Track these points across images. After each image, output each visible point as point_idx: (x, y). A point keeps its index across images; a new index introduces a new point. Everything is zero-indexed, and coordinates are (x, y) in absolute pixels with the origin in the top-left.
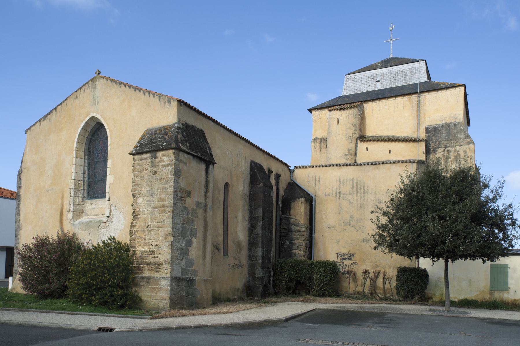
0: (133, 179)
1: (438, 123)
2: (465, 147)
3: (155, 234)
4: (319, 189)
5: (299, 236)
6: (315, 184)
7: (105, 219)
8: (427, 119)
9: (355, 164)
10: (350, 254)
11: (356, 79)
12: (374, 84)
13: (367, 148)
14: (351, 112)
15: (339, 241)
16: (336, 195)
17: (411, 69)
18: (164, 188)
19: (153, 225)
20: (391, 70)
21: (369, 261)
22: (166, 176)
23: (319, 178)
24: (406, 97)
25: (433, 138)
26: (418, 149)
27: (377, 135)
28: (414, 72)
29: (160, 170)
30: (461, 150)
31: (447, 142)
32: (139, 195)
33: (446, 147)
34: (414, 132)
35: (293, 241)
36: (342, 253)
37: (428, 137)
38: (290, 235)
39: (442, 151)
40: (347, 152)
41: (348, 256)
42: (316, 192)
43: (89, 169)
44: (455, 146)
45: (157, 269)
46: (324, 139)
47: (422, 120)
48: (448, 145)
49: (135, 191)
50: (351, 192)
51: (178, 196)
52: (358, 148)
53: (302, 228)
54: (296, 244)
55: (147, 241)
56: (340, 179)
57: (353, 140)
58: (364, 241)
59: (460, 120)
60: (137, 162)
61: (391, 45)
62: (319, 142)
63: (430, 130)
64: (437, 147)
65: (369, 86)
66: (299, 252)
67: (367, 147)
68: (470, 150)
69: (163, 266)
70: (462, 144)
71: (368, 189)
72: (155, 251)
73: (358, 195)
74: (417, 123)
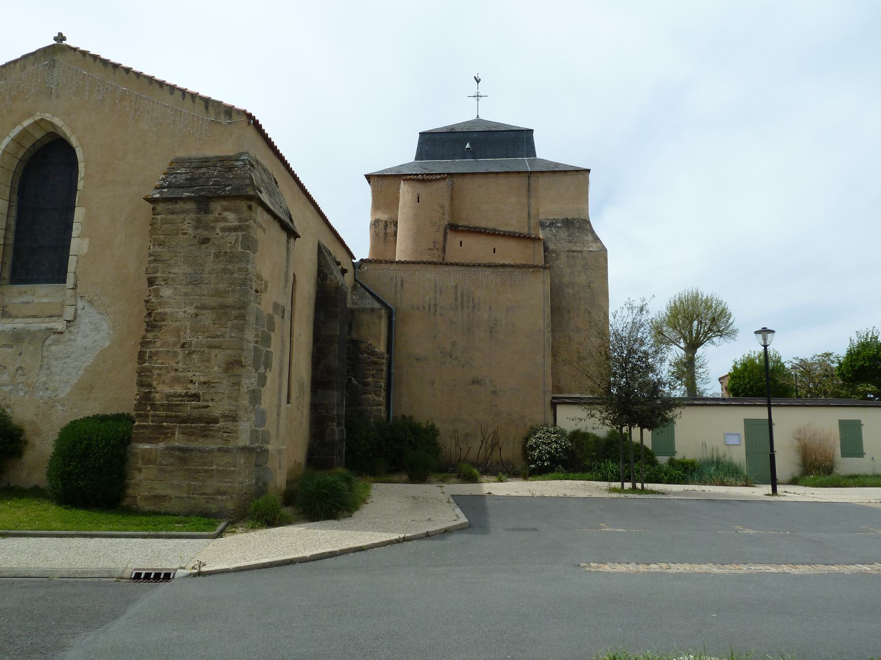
0: (151, 250)
3: (202, 361)
5: (375, 372)
7: (59, 326)
9: (444, 264)
13: (461, 242)
15: (434, 382)
18: (225, 271)
19: (197, 342)
22: (231, 248)
29: (217, 237)
32: (163, 280)
40: (432, 245)
43: (18, 223)
45: (205, 431)
49: (157, 272)
51: (252, 289)
52: (448, 241)
55: (180, 374)
60: (163, 216)
69: (218, 425)
71: (479, 303)
72: (201, 394)
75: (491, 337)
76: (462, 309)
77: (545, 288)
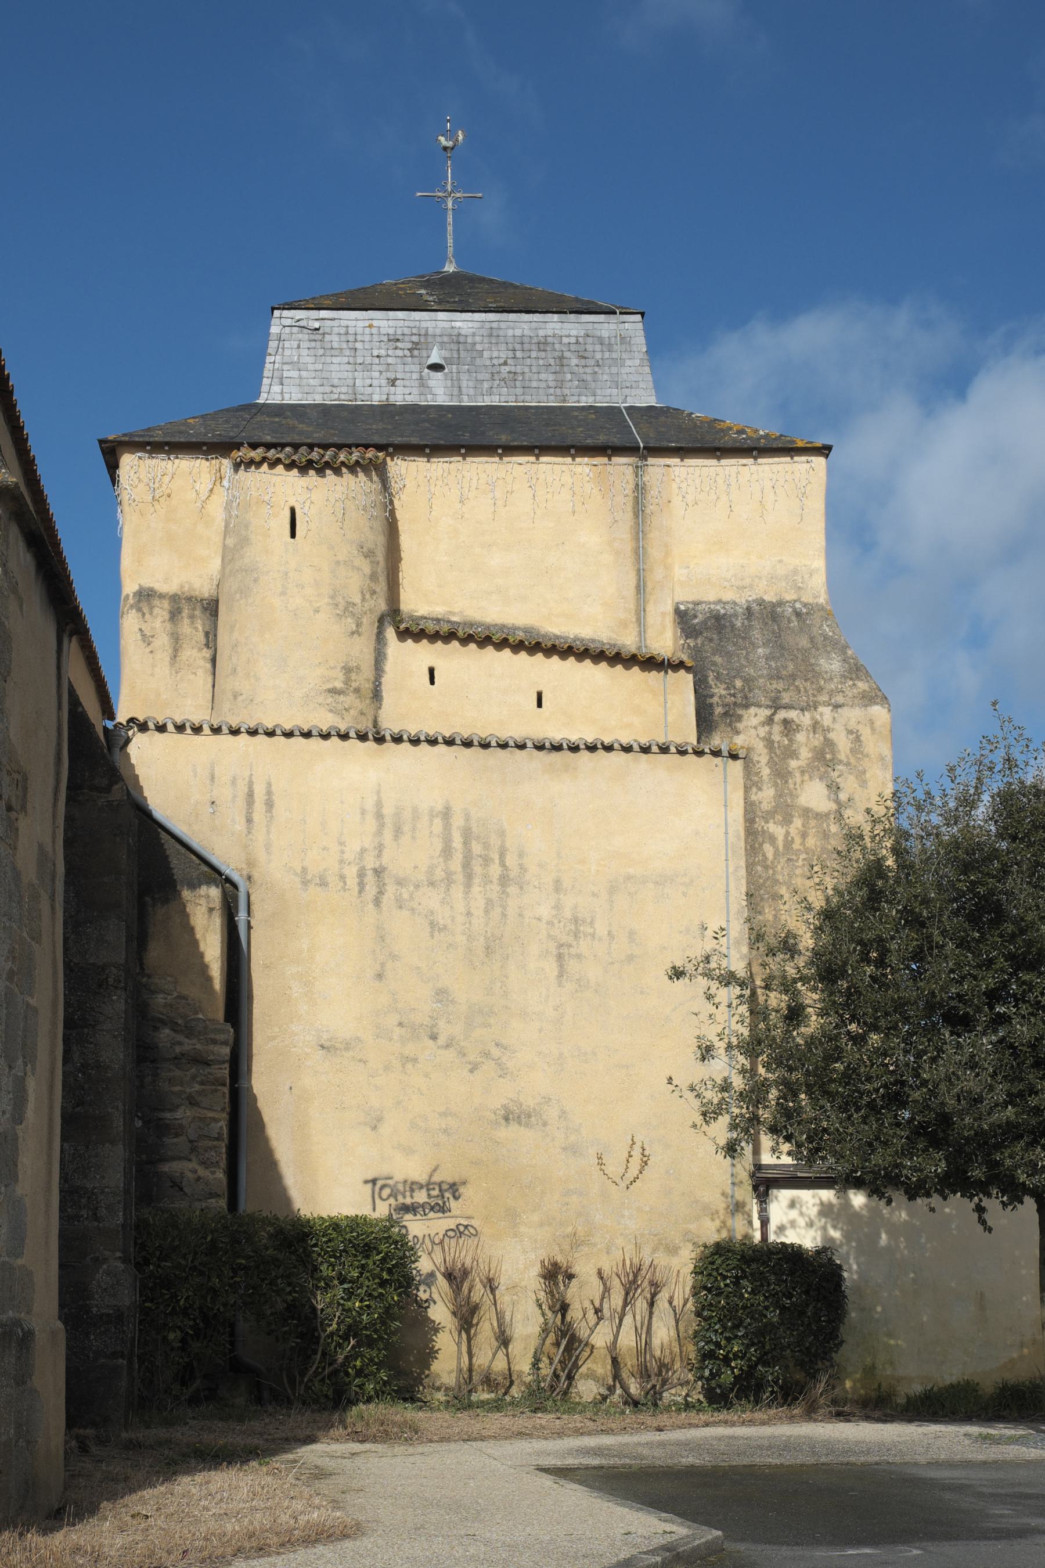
1: (728, 596)
2: (853, 715)
4: (268, 847)
5: (197, 1087)
6: (249, 821)
8: (679, 573)
10: (440, 1184)
11: (327, 338)
12: (415, 376)
13: (431, 671)
14: (352, 485)
15: (380, 1119)
16: (362, 886)
17: (581, 340)
20: (495, 325)
21: (535, 1218)
23: (269, 793)
24: (586, 460)
25: (718, 659)
26: (666, 702)
27: (453, 614)
28: (598, 356)
30: (837, 726)
31: (780, 686)
33: (776, 706)
34: (624, 624)
35: (168, 1115)
36: (399, 1177)
37: (696, 652)
38: (149, 1079)
39: (763, 724)
40: (341, 676)
41: (429, 1196)
42: (251, 863)
44: (816, 709)
46: (189, 599)
47: (657, 574)
48: (786, 698)
50: (439, 874)
52: (389, 666)
53: (214, 1042)
54: (181, 1126)
56: (379, 804)
57: (364, 620)
58: (507, 1119)
59: (815, 597)
61: (450, 219)
62: (167, 616)
63: (696, 621)
64: (739, 701)
65: (393, 382)
66: (202, 1172)
67: (431, 665)
68: (873, 730)
70: (839, 699)
71: (521, 866)
73: (476, 889)
74: (633, 582)
75: (560, 976)
76: (468, 885)
77: (730, 820)
